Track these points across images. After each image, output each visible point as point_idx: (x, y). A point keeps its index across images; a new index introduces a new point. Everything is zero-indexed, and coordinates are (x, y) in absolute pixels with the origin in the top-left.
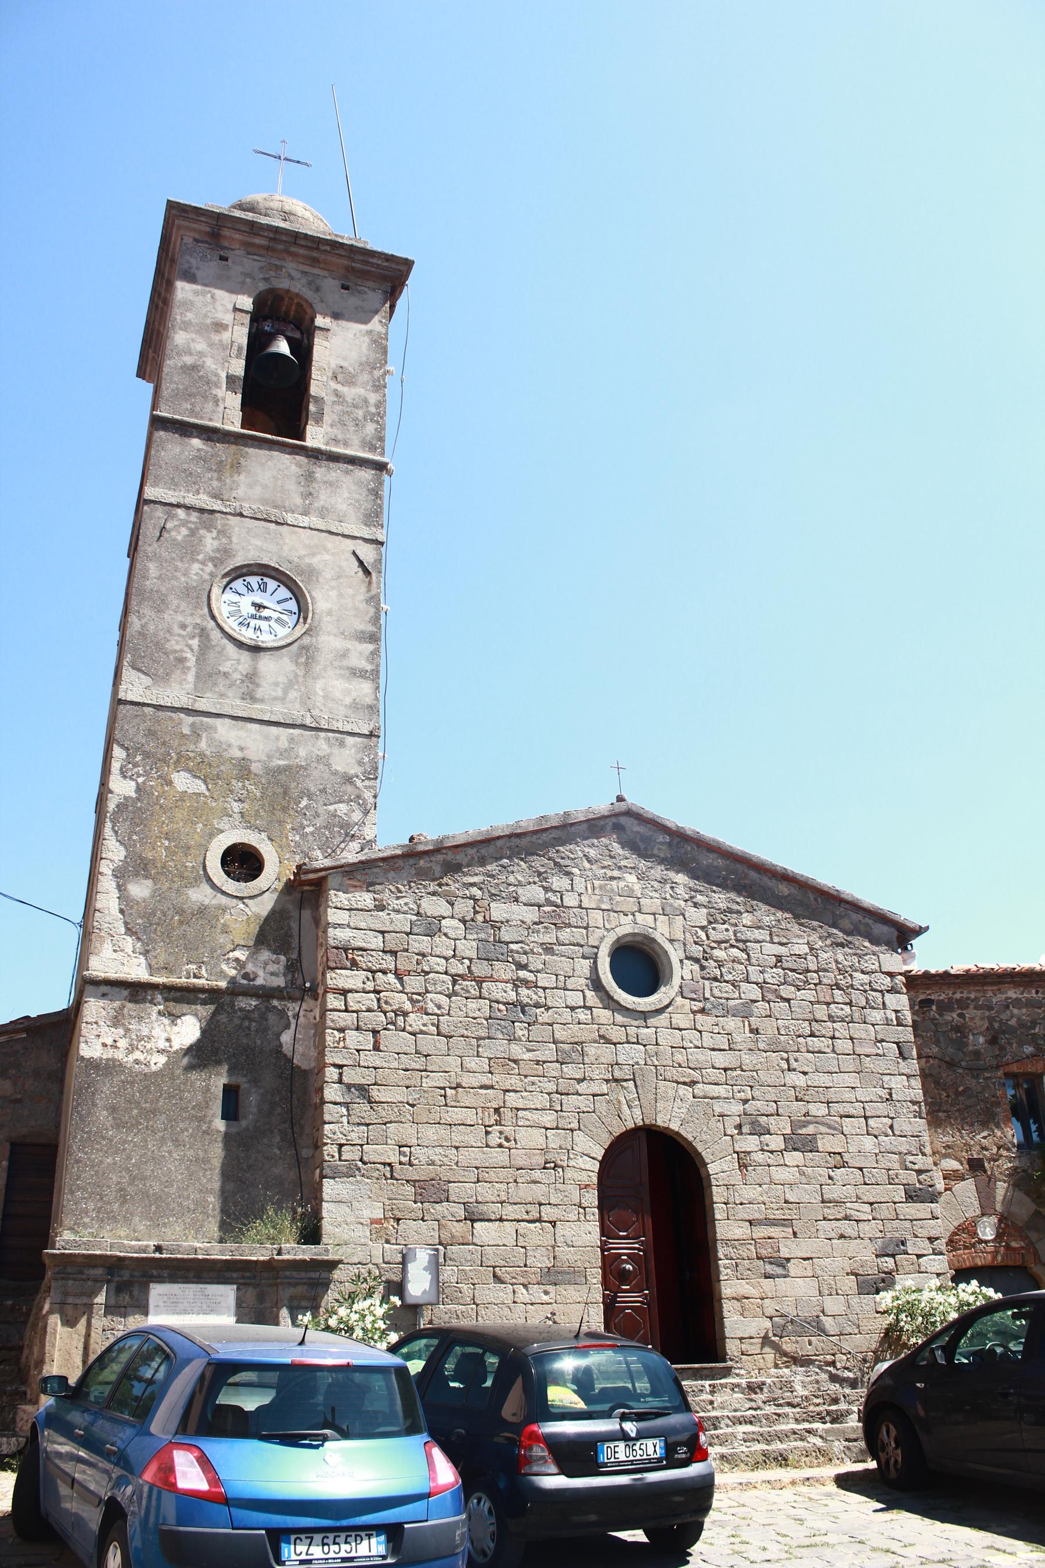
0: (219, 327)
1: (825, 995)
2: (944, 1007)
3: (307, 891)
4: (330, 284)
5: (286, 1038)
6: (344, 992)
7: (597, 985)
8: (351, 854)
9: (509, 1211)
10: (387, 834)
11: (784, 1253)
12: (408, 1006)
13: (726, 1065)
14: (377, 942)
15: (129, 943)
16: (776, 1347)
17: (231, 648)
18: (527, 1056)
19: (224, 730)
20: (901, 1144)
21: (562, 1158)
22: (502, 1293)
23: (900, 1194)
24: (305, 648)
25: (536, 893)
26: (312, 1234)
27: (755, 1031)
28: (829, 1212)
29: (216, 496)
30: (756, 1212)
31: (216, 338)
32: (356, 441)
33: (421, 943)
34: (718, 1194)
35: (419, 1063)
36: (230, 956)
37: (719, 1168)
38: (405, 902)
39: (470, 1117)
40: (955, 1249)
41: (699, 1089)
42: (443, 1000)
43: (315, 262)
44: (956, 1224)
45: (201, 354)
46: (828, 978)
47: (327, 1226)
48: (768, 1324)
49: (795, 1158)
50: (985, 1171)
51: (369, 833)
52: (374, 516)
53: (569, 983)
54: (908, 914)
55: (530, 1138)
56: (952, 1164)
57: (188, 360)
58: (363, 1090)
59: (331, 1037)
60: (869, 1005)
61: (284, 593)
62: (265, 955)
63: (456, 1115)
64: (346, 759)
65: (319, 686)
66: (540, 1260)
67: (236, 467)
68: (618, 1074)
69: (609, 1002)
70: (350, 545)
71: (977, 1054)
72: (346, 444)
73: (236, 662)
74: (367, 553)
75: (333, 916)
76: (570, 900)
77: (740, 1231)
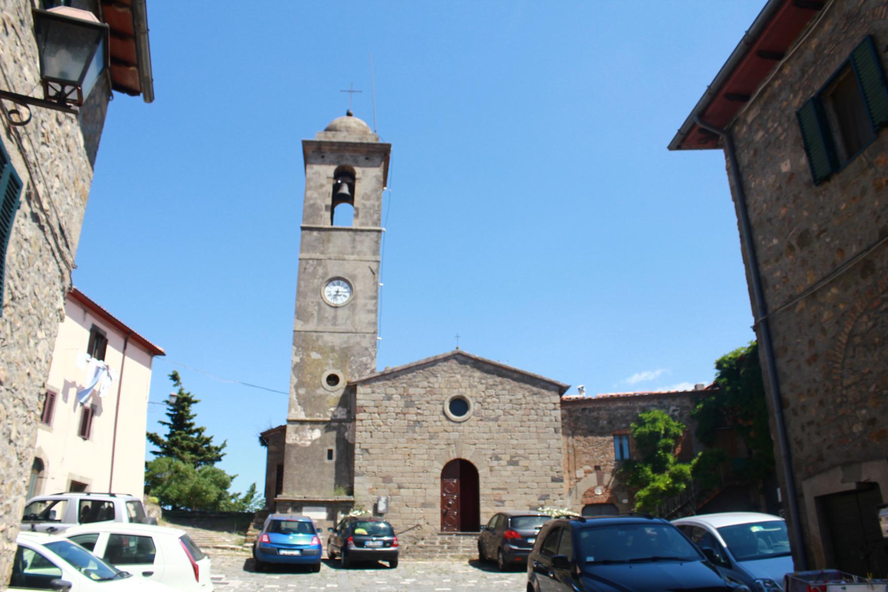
0: (322, 186)
1: (527, 412)
2: (591, 410)
3: (351, 389)
4: (362, 158)
5: (346, 434)
6: (361, 420)
7: (444, 413)
8: (366, 375)
9: (411, 486)
10: (380, 367)
11: (503, 498)
12: (381, 423)
14: (372, 404)
15: (299, 407)
17: (328, 308)
19: (327, 338)
21: (429, 470)
22: (409, 510)
23: (550, 479)
24: (353, 305)
25: (425, 384)
26: (351, 492)
27: (499, 426)
28: (521, 485)
29: (322, 253)
30: (495, 486)
31: (320, 191)
32: (370, 222)
33: (386, 403)
35: (385, 441)
36: (330, 411)
37: (482, 472)
38: (381, 388)
39: (400, 457)
41: (477, 446)
42: (393, 421)
43: (355, 151)
45: (316, 199)
46: (530, 406)
47: (356, 490)
49: (511, 467)
51: (373, 367)
52: (376, 252)
53: (435, 412)
54: (563, 382)
55: (419, 463)
56: (588, 468)
57: (312, 202)
58: (367, 450)
59: (358, 434)
60: (544, 415)
61: (346, 285)
62: (340, 409)
63: (395, 456)
64: (366, 343)
65: (357, 318)
66: (421, 500)
67: (329, 241)
69: (448, 418)
70: (367, 264)
71: (603, 428)
72: (367, 224)
73: (329, 313)
74: (374, 266)
75: (358, 396)
76: (436, 386)
77: (489, 492)
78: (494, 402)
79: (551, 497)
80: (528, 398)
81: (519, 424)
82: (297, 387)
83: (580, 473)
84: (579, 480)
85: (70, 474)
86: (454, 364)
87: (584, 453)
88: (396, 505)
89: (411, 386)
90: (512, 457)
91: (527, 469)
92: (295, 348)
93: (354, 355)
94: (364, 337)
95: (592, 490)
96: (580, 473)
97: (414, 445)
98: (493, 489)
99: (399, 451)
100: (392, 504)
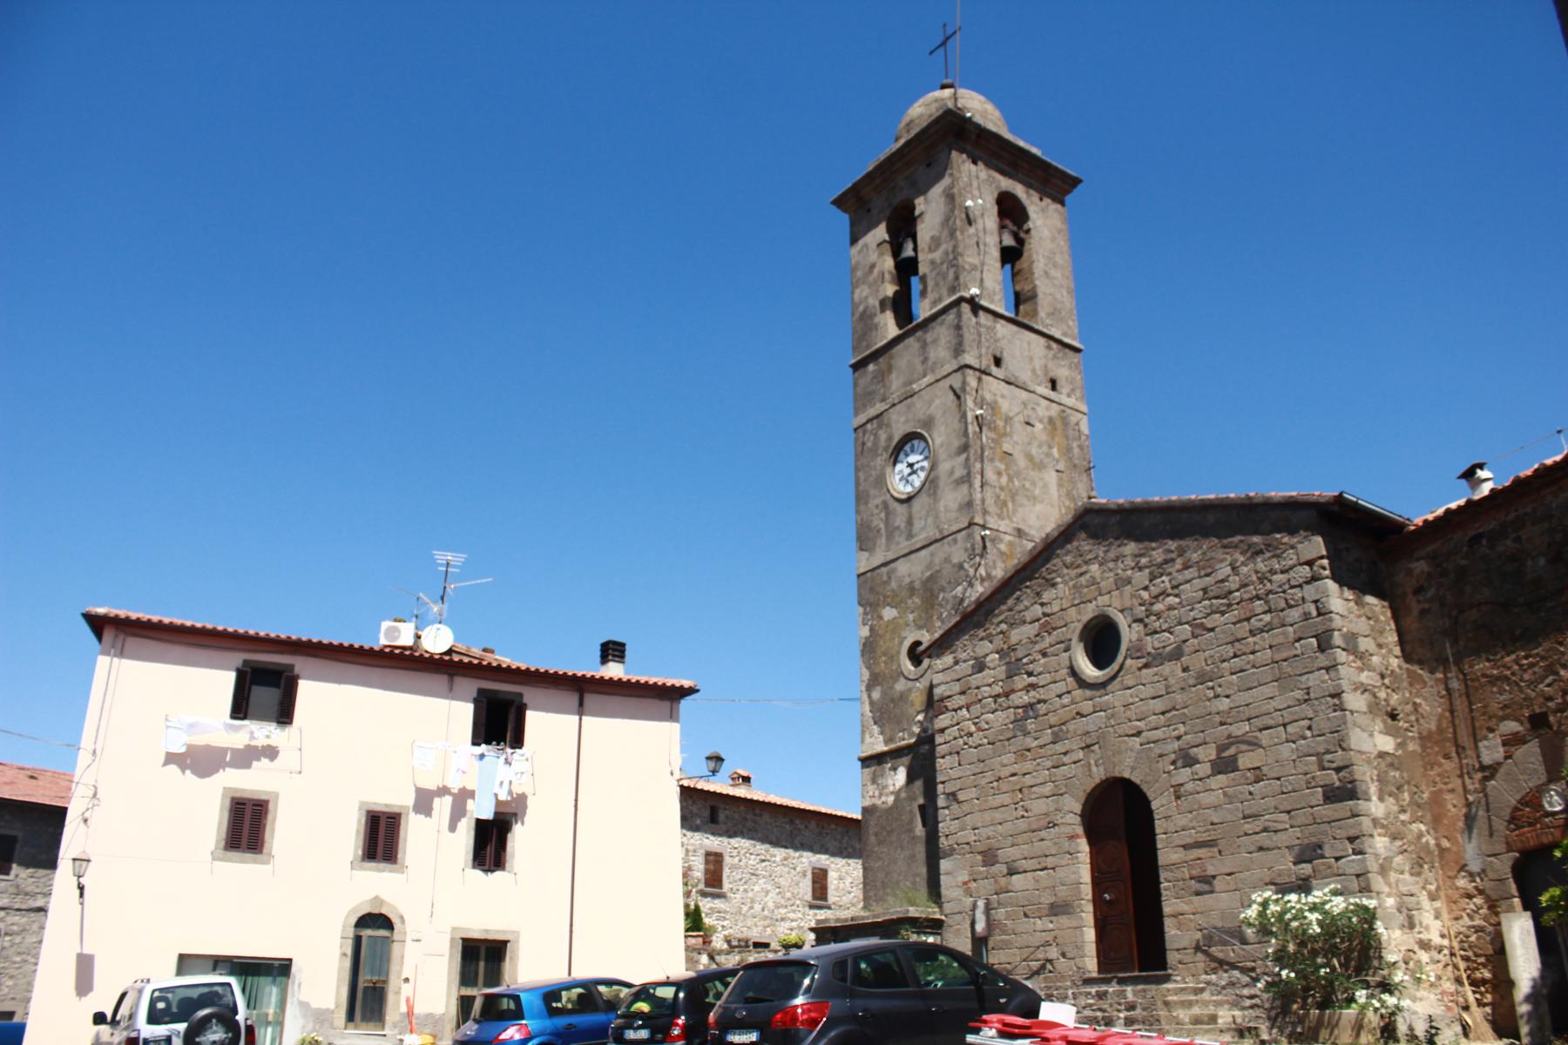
11: (1211, 871)
13: (1163, 709)
16: (1206, 953)
17: (896, 505)
18: (1036, 743)
19: (902, 568)
20: (1319, 743)
24: (932, 481)
25: (1038, 610)
27: (1185, 670)
28: (1248, 827)
30: (1189, 837)
34: (1159, 826)
37: (1160, 804)
39: (1006, 799)
40: (1518, 827)
44: (1518, 797)
48: (1199, 935)
49: (1222, 779)
50: (1550, 727)
56: (1511, 726)
63: (999, 799)
66: (1047, 899)
68: (1089, 741)
78: (1171, 608)
79: (1327, 852)
80: (1244, 570)
81: (1230, 651)
82: (869, 688)
83: (1491, 751)
84: (1490, 771)
85: (517, 933)
86: (1083, 544)
87: (1493, 681)
88: (1008, 916)
89: (1012, 626)
90: (1221, 748)
91: (1258, 775)
92: (861, 610)
93: (943, 589)
94: (955, 541)
95: (1532, 800)
96: (1491, 751)
97: (1028, 766)
98: (1185, 847)
99: (1004, 786)
100: (999, 914)
